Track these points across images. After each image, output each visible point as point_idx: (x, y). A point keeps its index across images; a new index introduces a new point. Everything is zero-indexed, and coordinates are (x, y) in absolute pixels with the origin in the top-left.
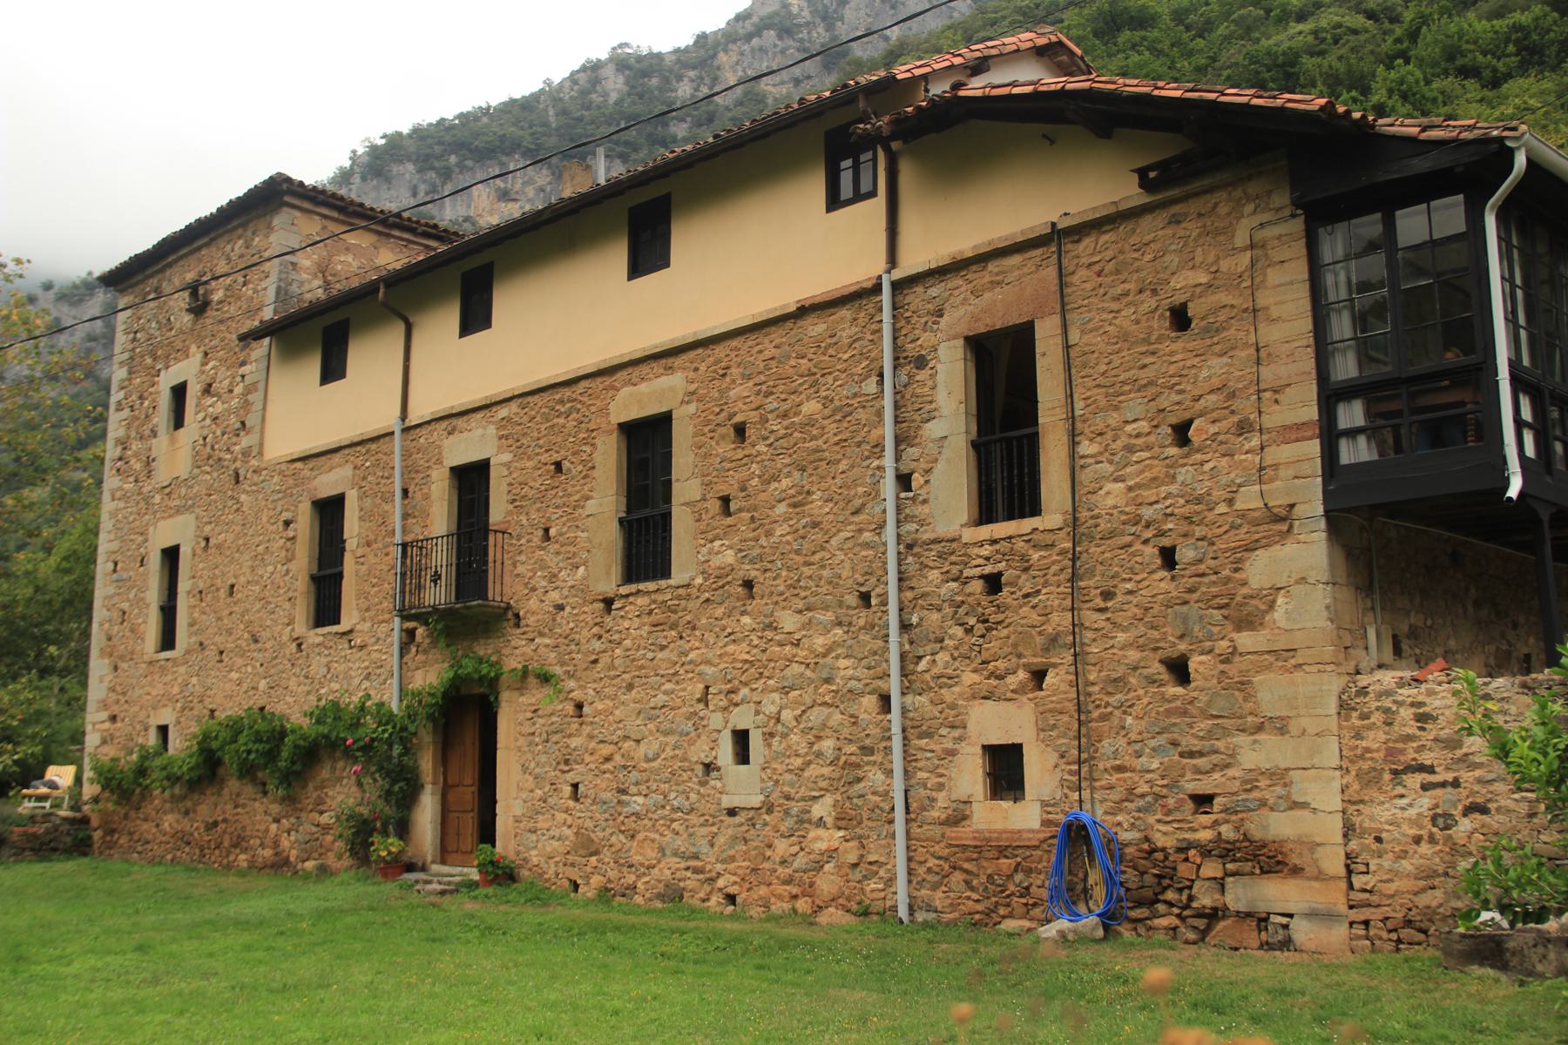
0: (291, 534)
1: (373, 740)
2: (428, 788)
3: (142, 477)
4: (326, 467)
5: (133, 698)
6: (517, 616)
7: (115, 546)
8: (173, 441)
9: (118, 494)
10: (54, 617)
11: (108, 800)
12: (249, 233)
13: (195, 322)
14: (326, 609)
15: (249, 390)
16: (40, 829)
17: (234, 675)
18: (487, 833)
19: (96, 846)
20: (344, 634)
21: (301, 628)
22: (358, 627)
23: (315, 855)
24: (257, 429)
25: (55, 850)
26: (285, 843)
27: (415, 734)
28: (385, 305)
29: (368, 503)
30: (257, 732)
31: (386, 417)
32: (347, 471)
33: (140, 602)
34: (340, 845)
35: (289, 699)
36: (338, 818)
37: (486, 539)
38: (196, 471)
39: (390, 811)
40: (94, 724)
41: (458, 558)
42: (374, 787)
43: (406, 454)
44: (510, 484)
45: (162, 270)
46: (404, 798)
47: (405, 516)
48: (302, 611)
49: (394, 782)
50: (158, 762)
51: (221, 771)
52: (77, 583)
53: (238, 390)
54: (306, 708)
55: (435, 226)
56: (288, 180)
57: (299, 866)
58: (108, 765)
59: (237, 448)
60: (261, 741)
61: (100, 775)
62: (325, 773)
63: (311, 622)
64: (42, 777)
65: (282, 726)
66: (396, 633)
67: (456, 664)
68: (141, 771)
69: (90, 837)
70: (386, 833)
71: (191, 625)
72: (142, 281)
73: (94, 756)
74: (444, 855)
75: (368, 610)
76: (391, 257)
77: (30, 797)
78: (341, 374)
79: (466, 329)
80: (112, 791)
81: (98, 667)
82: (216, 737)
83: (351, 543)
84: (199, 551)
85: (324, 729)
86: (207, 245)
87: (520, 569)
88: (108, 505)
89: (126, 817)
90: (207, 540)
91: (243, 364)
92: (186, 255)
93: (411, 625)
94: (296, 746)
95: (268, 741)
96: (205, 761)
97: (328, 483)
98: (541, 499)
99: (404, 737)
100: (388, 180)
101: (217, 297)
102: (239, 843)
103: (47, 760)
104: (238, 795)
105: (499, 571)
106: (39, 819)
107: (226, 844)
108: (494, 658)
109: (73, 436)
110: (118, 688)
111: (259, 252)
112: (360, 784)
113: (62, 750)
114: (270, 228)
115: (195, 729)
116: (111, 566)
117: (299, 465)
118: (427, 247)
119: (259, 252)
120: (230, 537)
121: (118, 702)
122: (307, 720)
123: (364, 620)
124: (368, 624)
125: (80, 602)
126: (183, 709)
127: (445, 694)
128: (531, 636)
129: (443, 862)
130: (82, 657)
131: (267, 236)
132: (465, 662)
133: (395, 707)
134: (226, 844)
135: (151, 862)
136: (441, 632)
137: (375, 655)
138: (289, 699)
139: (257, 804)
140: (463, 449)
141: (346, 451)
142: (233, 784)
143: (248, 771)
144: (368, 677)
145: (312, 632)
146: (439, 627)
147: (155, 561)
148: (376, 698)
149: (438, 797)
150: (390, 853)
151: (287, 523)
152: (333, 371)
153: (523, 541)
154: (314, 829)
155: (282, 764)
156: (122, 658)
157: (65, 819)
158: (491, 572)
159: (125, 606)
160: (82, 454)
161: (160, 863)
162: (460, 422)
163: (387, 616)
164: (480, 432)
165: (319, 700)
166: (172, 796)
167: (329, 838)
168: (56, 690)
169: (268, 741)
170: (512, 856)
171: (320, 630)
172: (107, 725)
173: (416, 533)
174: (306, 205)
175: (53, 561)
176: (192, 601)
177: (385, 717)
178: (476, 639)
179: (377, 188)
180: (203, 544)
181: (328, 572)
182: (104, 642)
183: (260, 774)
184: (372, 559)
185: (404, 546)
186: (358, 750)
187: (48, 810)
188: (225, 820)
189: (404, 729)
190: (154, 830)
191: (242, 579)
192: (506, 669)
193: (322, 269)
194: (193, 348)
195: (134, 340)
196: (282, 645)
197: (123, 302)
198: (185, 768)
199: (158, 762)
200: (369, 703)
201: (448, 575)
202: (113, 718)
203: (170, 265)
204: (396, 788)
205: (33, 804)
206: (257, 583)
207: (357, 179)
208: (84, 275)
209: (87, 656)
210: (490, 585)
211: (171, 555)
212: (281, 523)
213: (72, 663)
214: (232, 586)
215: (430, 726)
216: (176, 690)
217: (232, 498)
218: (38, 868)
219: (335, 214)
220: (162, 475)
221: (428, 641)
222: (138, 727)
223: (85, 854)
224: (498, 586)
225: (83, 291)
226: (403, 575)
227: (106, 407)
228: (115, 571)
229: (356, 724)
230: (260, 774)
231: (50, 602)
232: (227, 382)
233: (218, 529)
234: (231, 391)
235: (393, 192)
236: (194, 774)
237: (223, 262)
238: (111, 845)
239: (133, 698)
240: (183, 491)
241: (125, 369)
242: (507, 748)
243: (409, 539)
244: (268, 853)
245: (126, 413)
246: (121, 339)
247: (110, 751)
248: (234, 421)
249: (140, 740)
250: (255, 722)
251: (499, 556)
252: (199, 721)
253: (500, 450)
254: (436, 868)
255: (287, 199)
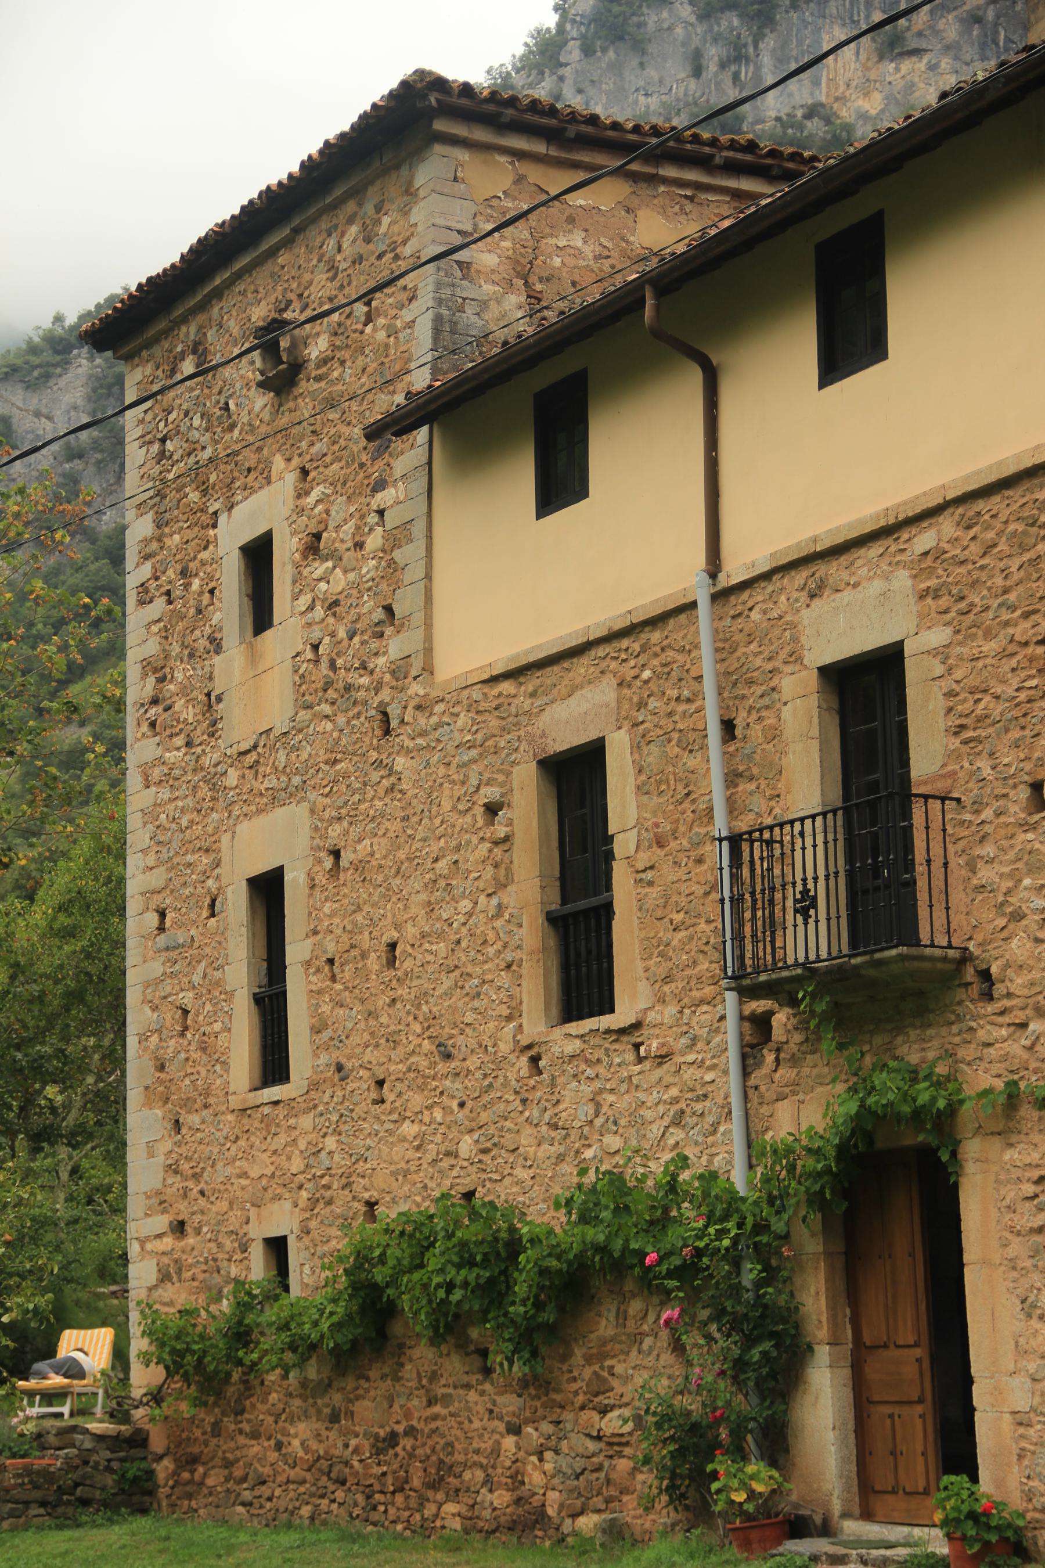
0: (501, 831)
1: (699, 1253)
2: (823, 1353)
3: (199, 736)
4: (562, 689)
5: (222, 1184)
6: (985, 975)
7: (157, 878)
8: (253, 657)
9: (156, 773)
10: (50, 1027)
11: (180, 1396)
12: (369, 208)
13: (277, 411)
14: (584, 982)
15: (395, 540)
16: (54, 1461)
17: (409, 1129)
18: (958, 1452)
19: (163, 1492)
20: (622, 1031)
21: (535, 1025)
22: (652, 1017)
23: (598, 1502)
24: (418, 618)
25: (85, 1502)
26: (535, 1478)
27: (786, 1237)
28: (658, 334)
29: (653, 755)
30: (463, 1244)
31: (681, 574)
32: (605, 692)
33: (215, 989)
34: (646, 1478)
35: (523, 1174)
36: (638, 1419)
37: (907, 815)
38: (304, 715)
39: (745, 1404)
40: (142, 1242)
41: (850, 859)
42: (710, 1353)
43: (724, 648)
44: (950, 694)
45: (203, 306)
46: (773, 1375)
47: (732, 778)
48: (534, 988)
49: (750, 1341)
50: (271, 1314)
51: (397, 1328)
52: (88, 956)
53: (374, 541)
54: (557, 1190)
55: (752, 146)
56: (439, 84)
57: (567, 1526)
58: (176, 1323)
59: (381, 661)
60: (472, 1264)
61: (162, 1345)
62: (604, 1326)
63: (555, 1011)
64: (50, 1352)
65: (512, 1230)
66: (731, 1024)
67: (860, 1086)
68: (241, 1335)
69: (151, 1473)
70: (740, 1454)
71: (316, 1030)
72: (166, 333)
73: (147, 1306)
74: (868, 1498)
75: (668, 979)
76: (664, 227)
77: (31, 1394)
78: (580, 492)
79: (834, 366)
80: (186, 1377)
81: (143, 1124)
82: (382, 1260)
83: (624, 844)
84: (321, 879)
85: (596, 1234)
86: (287, 243)
87: (986, 874)
88: (138, 798)
89: (217, 1430)
90: (336, 854)
91: (380, 486)
92: (248, 270)
93: (759, 1006)
94: (543, 1272)
95: (486, 1262)
96: (363, 1310)
97: (569, 718)
98: (1021, 721)
99: (764, 1244)
100: (639, 46)
101: (317, 348)
102: (442, 1478)
103: (62, 1318)
104: (434, 1377)
105: (938, 882)
106: (51, 1439)
107: (416, 1483)
108: (941, 1069)
109: (60, 660)
110: (185, 1166)
111: (393, 247)
112: (678, 1348)
113: (84, 1296)
114: (409, 192)
115: (340, 1243)
116: (153, 919)
117: (507, 687)
118: (737, 195)
119: (393, 247)
120: (381, 845)
121: (185, 1193)
122: (562, 1215)
123: (662, 1000)
124: (671, 1010)
125: (98, 995)
126: (314, 1201)
127: (842, 1150)
128: (1020, 1017)
129: (867, 1515)
130: (110, 1105)
131: (405, 212)
132: (879, 1079)
133: (740, 1187)
134: (416, 1483)
135: (271, 1523)
136: (824, 1018)
137: (689, 1074)
138: (523, 1174)
139: (472, 1396)
140: (845, 625)
141: (601, 651)
142: (422, 1355)
143: (449, 1328)
144: (678, 1121)
145: (559, 1032)
146: (820, 1007)
147: (237, 903)
148: (699, 1165)
149: (847, 1372)
150: (752, 1495)
151: (492, 810)
152: (560, 484)
153: (987, 814)
154: (592, 1446)
155: (517, 1310)
156: (187, 1103)
157: (100, 1438)
158: (921, 884)
159: (187, 998)
160: (74, 691)
161: (289, 1526)
162: (834, 570)
163: (709, 991)
164: (878, 585)
165: (583, 1172)
166: (304, 1384)
167: (623, 1465)
168: (64, 1176)
169: (486, 1262)
170: (1017, 1502)
171: (574, 1028)
172: (168, 1242)
173: (759, 811)
174: (480, 134)
175: (39, 914)
176: (317, 981)
177: (723, 1206)
178: (899, 1029)
179: (616, 68)
180: (329, 862)
181: (583, 904)
182: (151, 1075)
183: (474, 1333)
184: (669, 873)
185: (735, 841)
186: (670, 1275)
187: (67, 1421)
188: (411, 1432)
189: (762, 1227)
190: (273, 1456)
191: (411, 931)
192: (969, 1091)
193: (523, 272)
194: (278, 463)
195: (162, 455)
196: (500, 1062)
197: (135, 379)
198: (325, 1326)
199: (271, 1314)
200: (685, 1176)
201: (831, 898)
202: (179, 1228)
203: (218, 294)
204: (755, 1355)
205: (35, 1411)
206: (441, 935)
207: (573, 53)
208: (47, 324)
209: (121, 1102)
210: (923, 913)
211: (268, 889)
212: (479, 810)
213: (91, 1118)
214: (392, 946)
215: (816, 1218)
216: (296, 1164)
217: (378, 764)
218: (57, 1540)
219: (540, 147)
220: (239, 727)
221: (798, 1037)
222: (228, 1244)
223: (144, 1511)
224: (939, 915)
225: (48, 356)
226: (737, 901)
227: (118, 594)
228: (161, 929)
229: (660, 1221)
230: (474, 1333)
231: (41, 998)
232: (349, 527)
233: (354, 832)
234: (359, 545)
235: (652, 73)
236: (344, 1337)
237: (321, 277)
238: (191, 1490)
239: (222, 1184)
240: (282, 756)
241: (150, 516)
242: (985, 1262)
243: (742, 825)
244: (501, 1498)
245: (158, 607)
246: (135, 454)
247: (178, 1296)
248: (370, 609)
249: (234, 1271)
250: (457, 1223)
251: (937, 850)
252: (345, 1227)
253: (924, 622)
254: (852, 1527)
255: (440, 125)
